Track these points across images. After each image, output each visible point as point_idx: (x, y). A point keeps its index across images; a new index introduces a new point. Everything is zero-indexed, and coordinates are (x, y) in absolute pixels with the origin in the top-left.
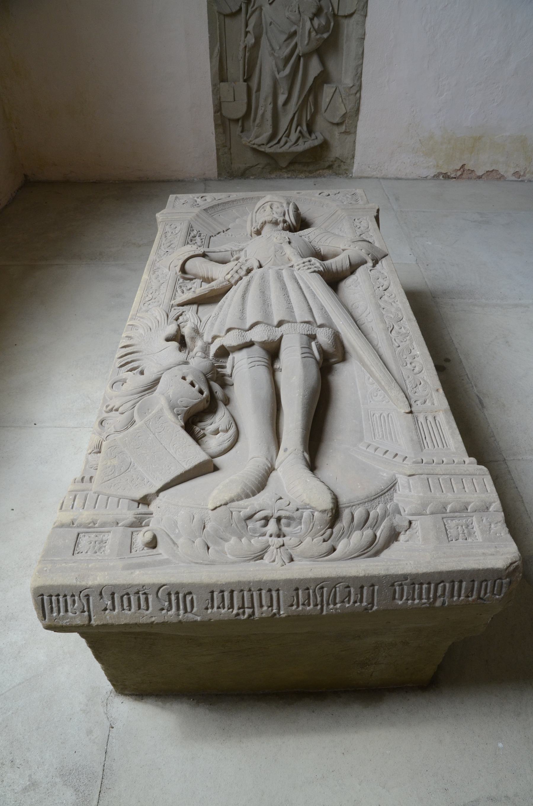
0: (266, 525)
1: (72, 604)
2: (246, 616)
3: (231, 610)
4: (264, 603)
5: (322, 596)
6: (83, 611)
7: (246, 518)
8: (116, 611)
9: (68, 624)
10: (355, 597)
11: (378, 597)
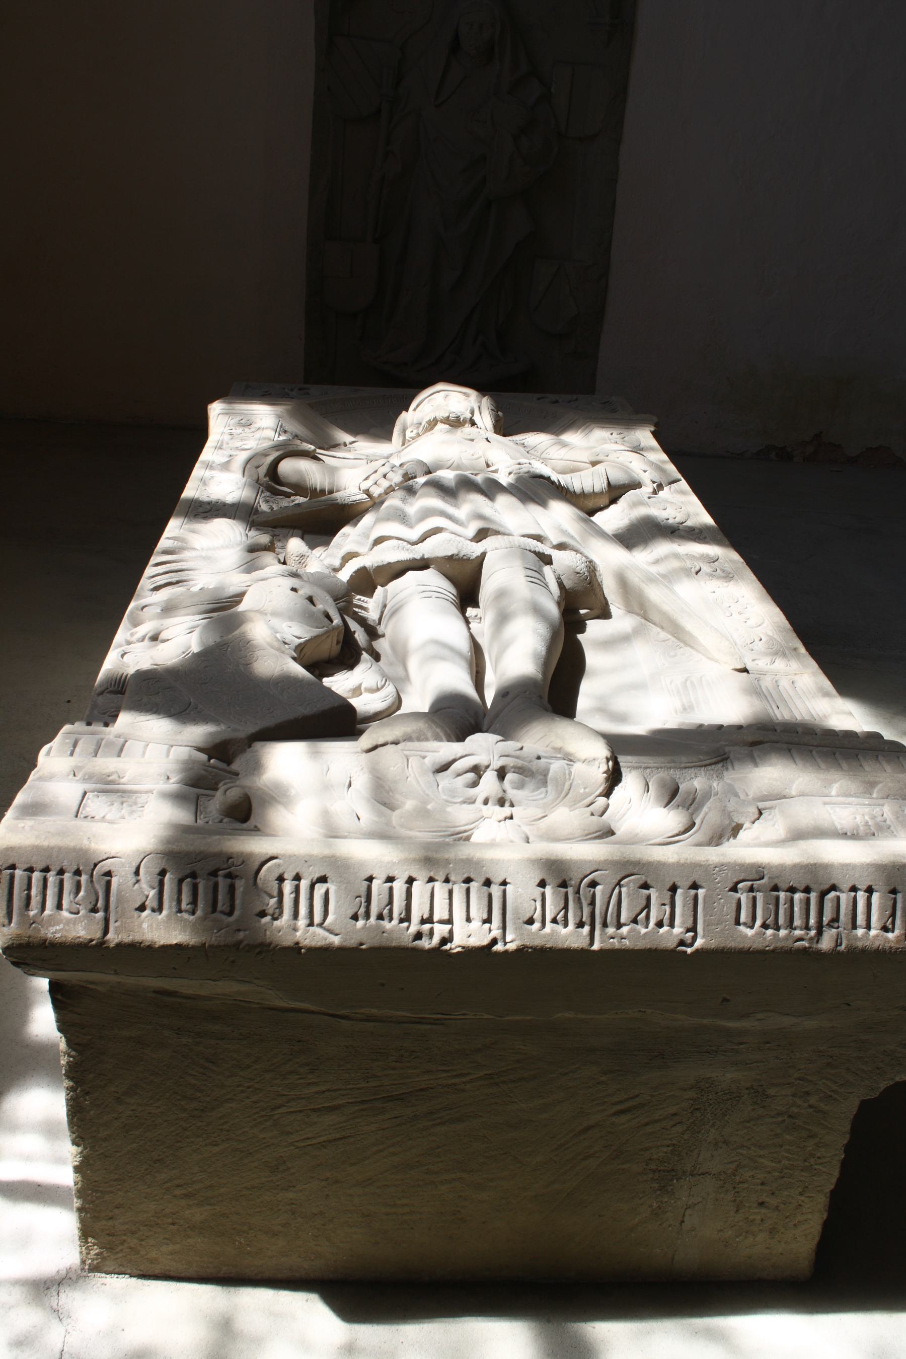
0: (475, 784)
1: (74, 890)
2: (436, 940)
3: (405, 924)
4: (473, 914)
5: (592, 903)
6: (94, 910)
7: (437, 767)
8: (165, 912)
9: (58, 935)
10: (659, 911)
11: (705, 915)
